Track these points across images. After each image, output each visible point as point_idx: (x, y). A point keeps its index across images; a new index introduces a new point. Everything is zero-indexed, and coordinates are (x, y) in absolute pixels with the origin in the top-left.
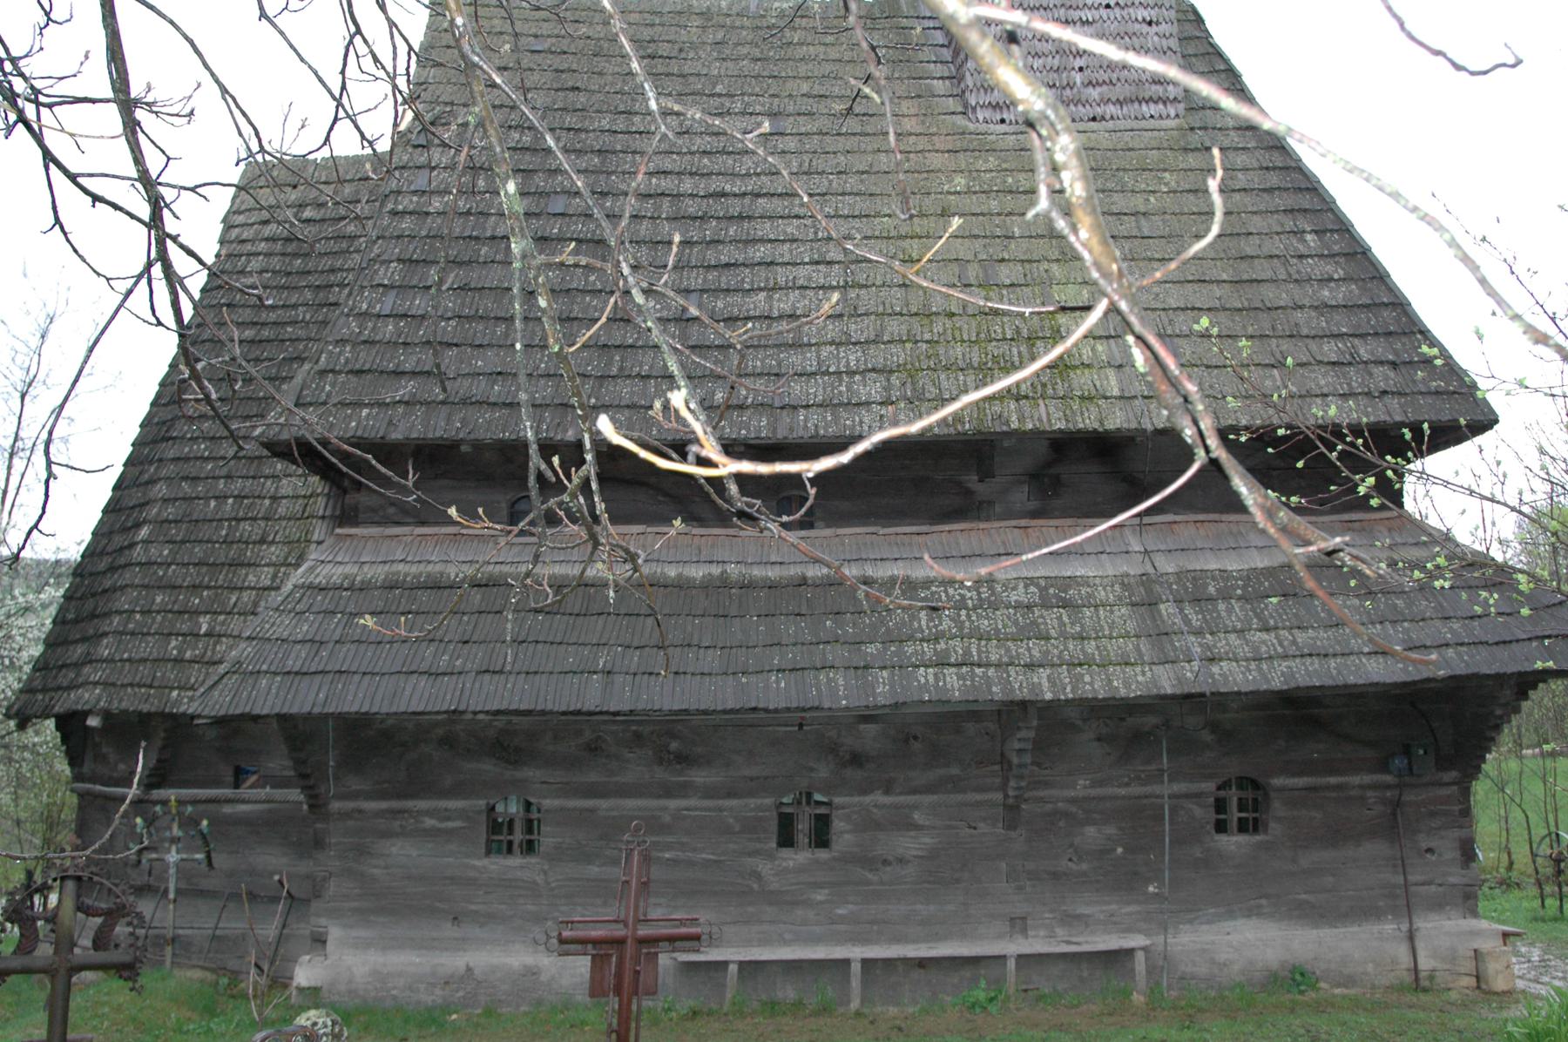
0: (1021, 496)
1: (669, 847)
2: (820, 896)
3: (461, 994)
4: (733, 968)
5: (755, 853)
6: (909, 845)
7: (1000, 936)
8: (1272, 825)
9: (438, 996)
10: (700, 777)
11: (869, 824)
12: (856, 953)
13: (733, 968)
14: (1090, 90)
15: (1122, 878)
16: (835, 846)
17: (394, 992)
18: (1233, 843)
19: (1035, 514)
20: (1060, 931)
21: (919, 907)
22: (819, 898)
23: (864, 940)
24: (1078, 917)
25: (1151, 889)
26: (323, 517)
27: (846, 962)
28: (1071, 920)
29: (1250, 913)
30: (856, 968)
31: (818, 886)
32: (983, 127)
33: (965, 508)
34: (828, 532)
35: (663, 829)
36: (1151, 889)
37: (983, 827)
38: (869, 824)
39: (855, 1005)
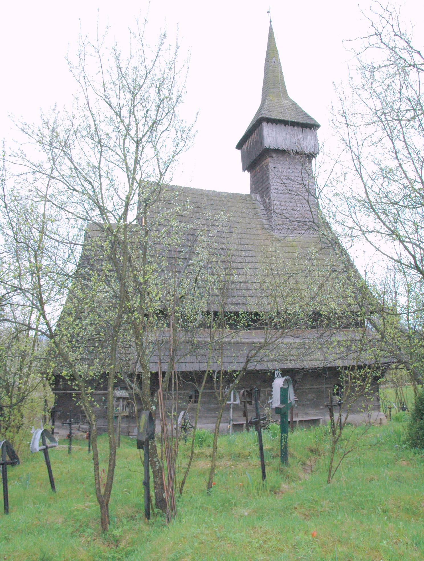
20: (304, 416)
28: (307, 414)
36: (321, 407)
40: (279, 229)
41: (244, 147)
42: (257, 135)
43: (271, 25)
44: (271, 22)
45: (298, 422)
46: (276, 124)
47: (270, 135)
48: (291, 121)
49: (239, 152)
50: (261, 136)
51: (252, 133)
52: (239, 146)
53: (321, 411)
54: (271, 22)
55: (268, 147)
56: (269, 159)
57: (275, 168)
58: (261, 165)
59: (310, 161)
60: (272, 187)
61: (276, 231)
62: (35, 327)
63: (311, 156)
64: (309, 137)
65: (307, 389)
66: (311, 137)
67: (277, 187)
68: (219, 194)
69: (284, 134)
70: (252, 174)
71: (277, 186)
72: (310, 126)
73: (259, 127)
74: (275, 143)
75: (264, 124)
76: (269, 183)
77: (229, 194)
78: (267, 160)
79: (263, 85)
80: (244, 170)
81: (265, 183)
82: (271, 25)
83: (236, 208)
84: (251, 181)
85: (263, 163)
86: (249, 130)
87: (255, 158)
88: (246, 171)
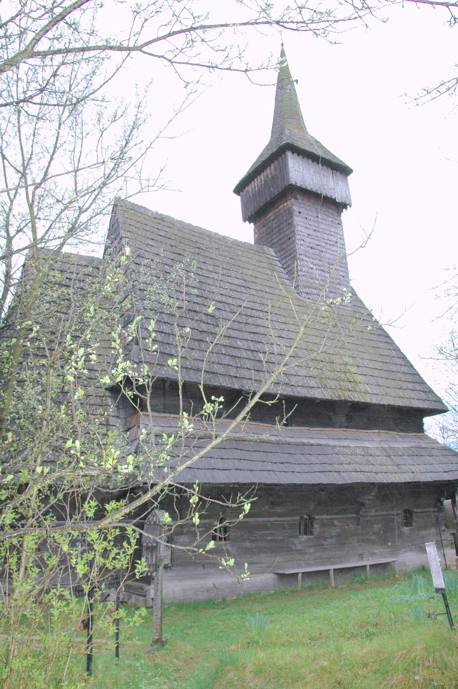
0: (343, 420)
1: (270, 535)
2: (311, 550)
3: (213, 594)
4: (300, 575)
5: (292, 537)
6: (334, 532)
7: (356, 561)
8: (414, 523)
9: (206, 596)
10: (279, 510)
11: (323, 525)
12: (331, 567)
13: (300, 575)
14: (330, 294)
15: (383, 540)
16: (315, 533)
17: (190, 596)
18: (405, 529)
19: (347, 427)
20: (370, 558)
21: (337, 552)
22: (311, 551)
23: (333, 563)
24: (375, 554)
25: (390, 544)
26: (22, 402)
27: (329, 570)
28: (373, 554)
29: (411, 550)
30: (332, 572)
31: (310, 547)
32: (304, 299)
33: (328, 423)
34: (297, 428)
35: (267, 528)
36: (390, 544)
37: (351, 526)
38: (323, 525)
39: (333, 585)
40: (307, 293)
41: (249, 188)
42: (275, 169)
43: (283, 48)
44: (282, 45)
45: (368, 568)
46: (303, 158)
47: (296, 168)
48: (322, 158)
49: (238, 199)
50: (284, 170)
51: (269, 165)
52: (239, 189)
53: (390, 549)
54: (282, 45)
55: (294, 183)
56: (293, 200)
57: (300, 213)
58: (277, 210)
59: (339, 213)
60: (298, 237)
61: (304, 295)
62: (443, 538)
63: (343, 206)
64: (340, 183)
65: (372, 516)
66: (342, 183)
67: (303, 238)
68: (224, 239)
69: (312, 171)
70: (258, 224)
71: (304, 236)
72: (342, 170)
73: (280, 159)
74: (288, 187)
75: (289, 154)
76: (294, 232)
77: (235, 241)
78: (289, 202)
79: (274, 116)
80: (245, 221)
81: (284, 232)
82: (283, 48)
83: (249, 260)
84: (255, 233)
85: (282, 206)
86: (249, 174)
87: (269, 199)
88: (247, 222)
